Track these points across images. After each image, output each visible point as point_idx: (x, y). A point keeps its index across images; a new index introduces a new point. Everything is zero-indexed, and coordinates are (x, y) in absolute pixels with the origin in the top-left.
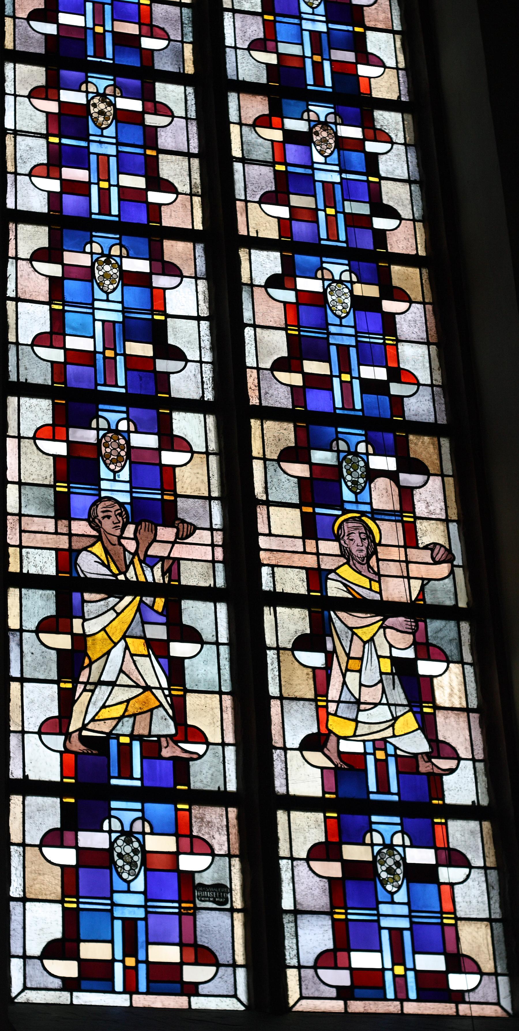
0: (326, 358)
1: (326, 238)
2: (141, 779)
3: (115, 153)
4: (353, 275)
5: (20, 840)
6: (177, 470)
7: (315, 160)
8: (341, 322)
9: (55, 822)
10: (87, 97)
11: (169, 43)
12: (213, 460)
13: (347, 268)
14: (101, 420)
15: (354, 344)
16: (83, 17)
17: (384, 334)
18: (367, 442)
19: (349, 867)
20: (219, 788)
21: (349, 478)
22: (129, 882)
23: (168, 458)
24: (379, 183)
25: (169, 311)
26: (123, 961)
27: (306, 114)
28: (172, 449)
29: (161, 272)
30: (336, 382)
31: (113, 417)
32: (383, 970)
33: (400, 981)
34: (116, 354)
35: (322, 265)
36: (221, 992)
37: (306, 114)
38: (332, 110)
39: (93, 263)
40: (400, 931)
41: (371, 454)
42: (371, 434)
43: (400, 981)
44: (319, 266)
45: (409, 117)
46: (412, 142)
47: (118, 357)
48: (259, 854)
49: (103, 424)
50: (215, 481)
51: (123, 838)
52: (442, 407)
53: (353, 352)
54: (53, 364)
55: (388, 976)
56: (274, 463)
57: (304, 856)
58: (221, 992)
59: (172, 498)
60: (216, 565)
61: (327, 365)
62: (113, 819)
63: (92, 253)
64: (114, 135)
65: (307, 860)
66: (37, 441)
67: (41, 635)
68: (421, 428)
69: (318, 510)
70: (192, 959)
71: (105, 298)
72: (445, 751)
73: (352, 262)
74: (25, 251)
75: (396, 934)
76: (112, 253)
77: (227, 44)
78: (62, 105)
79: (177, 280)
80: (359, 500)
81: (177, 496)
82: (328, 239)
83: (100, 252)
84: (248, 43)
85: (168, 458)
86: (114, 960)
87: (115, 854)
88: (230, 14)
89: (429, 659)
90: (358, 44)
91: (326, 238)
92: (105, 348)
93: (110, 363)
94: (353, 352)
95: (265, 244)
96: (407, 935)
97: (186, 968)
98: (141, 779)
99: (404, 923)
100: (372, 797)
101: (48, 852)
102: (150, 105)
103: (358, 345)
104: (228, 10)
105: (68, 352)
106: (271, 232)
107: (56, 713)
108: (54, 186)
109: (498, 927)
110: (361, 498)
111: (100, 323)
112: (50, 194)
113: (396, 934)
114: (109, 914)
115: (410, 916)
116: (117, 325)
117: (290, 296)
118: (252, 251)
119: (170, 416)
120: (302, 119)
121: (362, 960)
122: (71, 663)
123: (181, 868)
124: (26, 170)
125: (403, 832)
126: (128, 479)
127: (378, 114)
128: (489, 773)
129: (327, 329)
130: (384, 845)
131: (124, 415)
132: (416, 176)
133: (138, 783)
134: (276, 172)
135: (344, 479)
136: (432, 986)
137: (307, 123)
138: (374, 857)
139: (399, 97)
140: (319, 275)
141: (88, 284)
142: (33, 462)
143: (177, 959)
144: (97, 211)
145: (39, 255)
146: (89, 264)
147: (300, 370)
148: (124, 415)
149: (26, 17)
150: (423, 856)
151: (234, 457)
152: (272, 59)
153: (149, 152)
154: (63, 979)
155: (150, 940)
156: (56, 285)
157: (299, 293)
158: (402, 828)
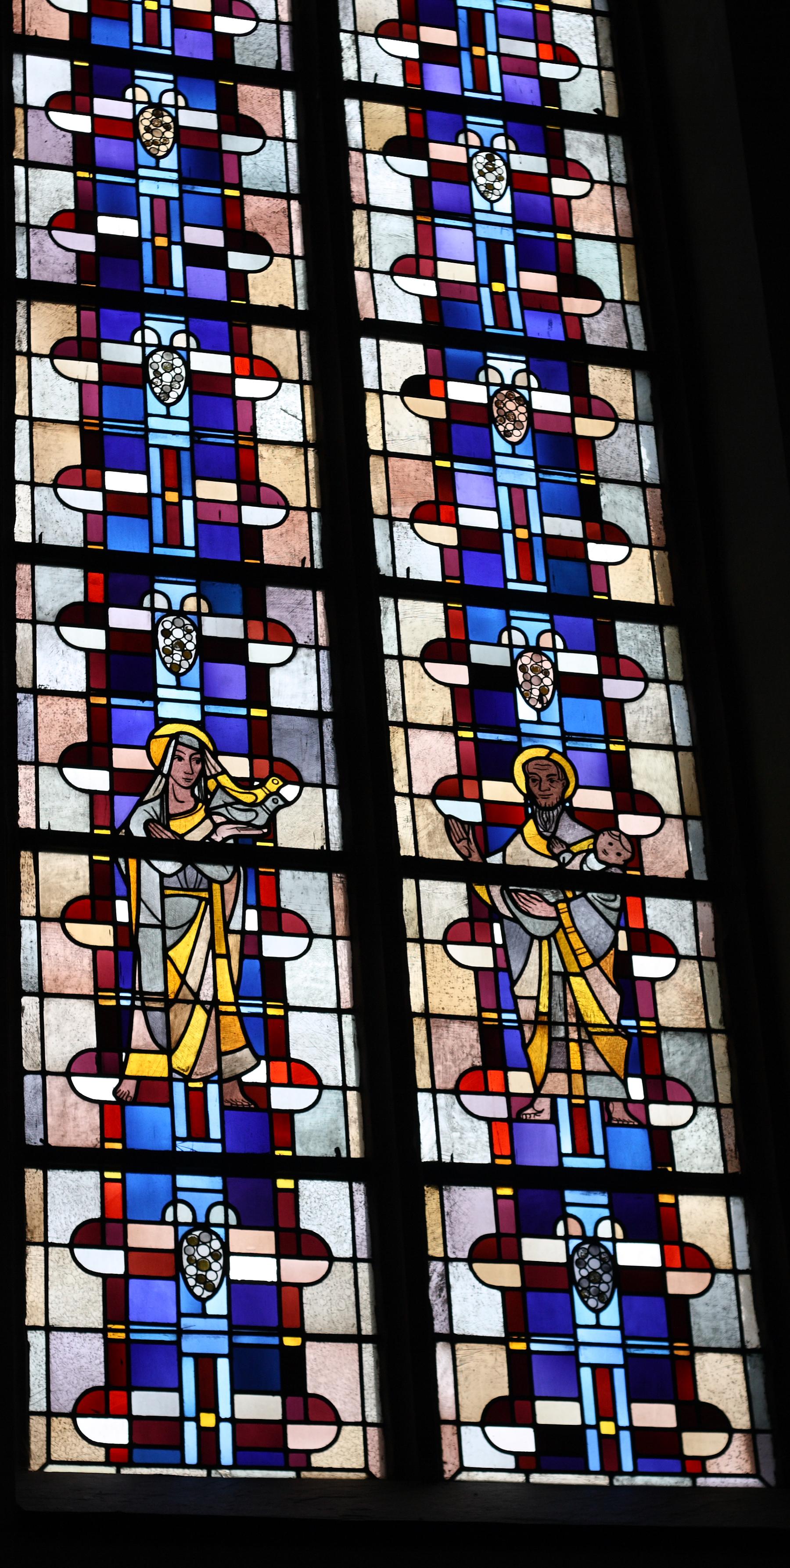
0: (452, 25)
1: (515, 577)
2: (222, 1141)
3: (226, 1350)
4: (511, 142)
5: (43, 1408)
6: (297, 1117)
7: (476, 206)
8: (492, 207)
9: (65, 84)
10: (144, 351)
11: (258, 37)
12: (364, 1269)
13: (501, 131)
14: (157, 596)
15: (534, 484)
16: (145, 477)
17: (671, 1339)
18: (507, 137)
19: (533, 1271)
20: (337, 1150)
21: (481, 180)
22: (203, 1301)
23: (252, 515)
24: (572, 243)
25: (310, 1326)
26: (197, 1419)
27: (505, 635)
28: (257, 502)
29: (285, 1081)
30: (508, 539)
31: (156, 89)
32: (584, 1427)
33: (609, 1444)
34: (171, 243)
35: (485, 362)
36: (343, 1452)
37: (505, 635)
38: (523, 366)
39: (178, 1243)
40: (609, 1368)
41: (560, 651)
42: (510, 125)
43: (609, 1444)
44: (482, 364)
45: (616, 142)
46: (662, 543)
47: (185, 502)
48: (357, 664)
49: (160, 602)
50: (366, 1311)
51: (151, 110)
52: (611, 91)
53: (510, 251)
54: (76, 135)
55: (592, 1437)
56: (406, 524)
57: (465, 1254)
58: (343, 1452)
59: (281, 1012)
60: (359, 1265)
61: (453, 34)
62: (146, 331)
63: (176, 1224)
64: (175, 167)
65: (470, 1260)
66: (59, 490)
67: (77, 1251)
68: (634, 612)
69: (534, 1347)
70: (261, 636)
71: (164, 412)
72: (672, 1089)
73: (531, 360)
74: (42, 343)
75: (602, 1372)
76: (186, 609)
77: (366, 386)
78: (113, 634)
79: (264, 259)
80: (543, 719)
81: (288, 1008)
82: (519, 580)
83: (156, 342)
84: (409, 510)
85: (252, 515)
86: (182, 1418)
87: (185, 1257)
88: (364, 214)
89: (618, 676)
90: (587, 507)
91: (515, 577)
92: (154, 234)
93: (161, 227)
94: (510, 251)
95: (420, 590)
96: (532, 495)
97: (239, 382)
98: (222, 1141)
99: (615, 1357)
100: (511, 586)
101: (84, 1255)
102: (296, 1402)
103: (518, 241)
104: (376, 453)
105: (97, 120)
106: (392, 76)
107: (93, 1043)
108: (93, 501)
109: (687, 758)
110: (546, 716)
111: (147, 199)
112: (77, 136)
113: (602, 1372)
114: (174, 1348)
115: (623, 1346)
116: (172, 202)
117: (420, 168)
118: (381, 342)
119: (234, 89)
120: (499, 644)
121: (554, 1413)
122: (118, 966)
123: (266, 953)
124: (49, 478)
125: (613, 1219)
126: (187, 415)
127: (571, 136)
128: (667, 502)
129: (574, 1336)
130: (584, 1237)
131: (171, 86)
132: (626, 231)
133: (217, 1148)
134: (436, 469)
135: (475, 182)
136: (655, 1446)
137: (507, 650)
138: (570, 1257)
139: (689, 873)
140: (482, 377)
141: (130, 144)
142: (58, 661)
143: (277, 1415)
144: (140, 41)
145: (61, 350)
146: (170, 1245)
147: (515, 1257)
148: (171, 86)
149: (67, 1242)
150: (641, 1255)
151: (357, 664)
152: (429, 288)
153: (255, 712)
154: (108, 1447)
155: (186, 220)
156: (114, 1291)
157: (452, 405)
158: (225, 1197)
